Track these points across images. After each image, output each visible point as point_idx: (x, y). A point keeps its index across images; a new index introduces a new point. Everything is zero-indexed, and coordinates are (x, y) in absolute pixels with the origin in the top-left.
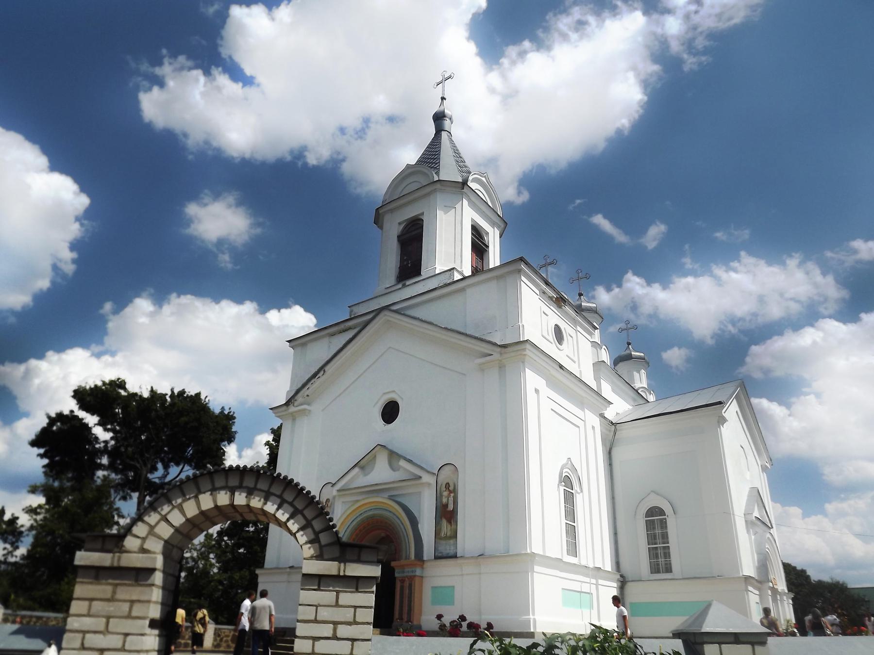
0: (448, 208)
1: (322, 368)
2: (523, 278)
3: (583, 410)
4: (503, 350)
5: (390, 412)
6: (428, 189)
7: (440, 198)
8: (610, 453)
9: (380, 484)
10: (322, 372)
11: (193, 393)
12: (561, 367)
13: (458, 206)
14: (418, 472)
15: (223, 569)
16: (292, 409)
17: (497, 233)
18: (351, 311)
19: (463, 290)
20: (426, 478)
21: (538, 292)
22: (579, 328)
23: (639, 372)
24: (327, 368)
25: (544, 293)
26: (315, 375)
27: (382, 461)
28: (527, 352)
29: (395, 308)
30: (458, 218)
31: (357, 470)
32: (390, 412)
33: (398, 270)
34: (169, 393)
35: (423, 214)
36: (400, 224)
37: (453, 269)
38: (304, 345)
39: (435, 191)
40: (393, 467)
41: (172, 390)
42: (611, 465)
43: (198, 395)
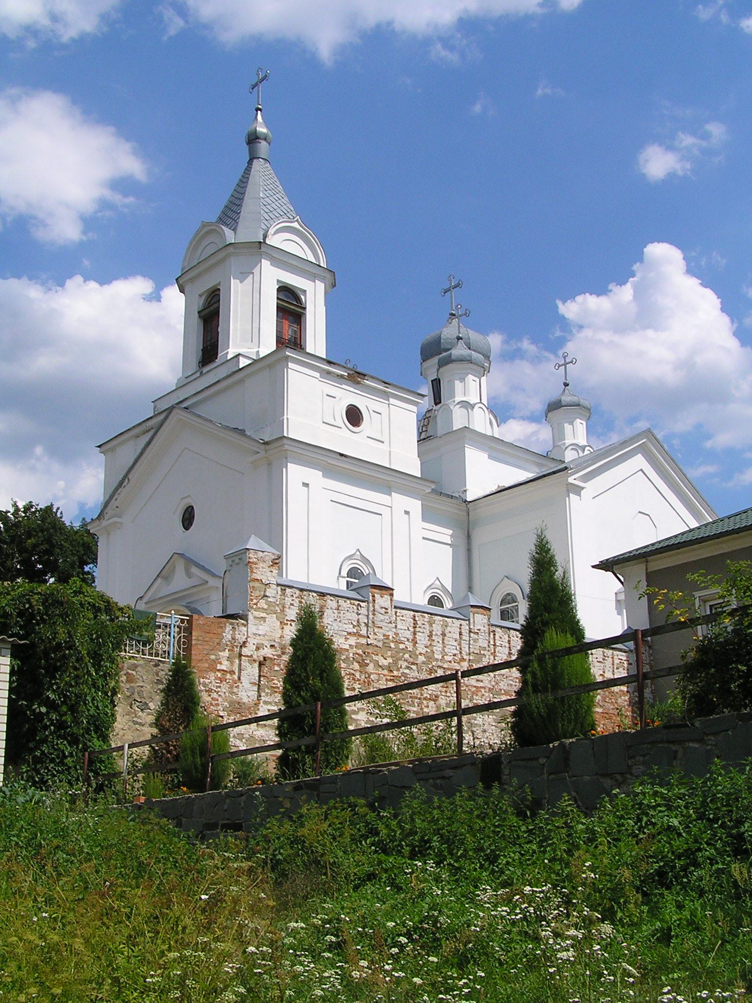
0: (243, 276)
1: (126, 476)
2: (291, 365)
3: (390, 495)
4: (267, 447)
5: (188, 518)
6: (221, 255)
7: (234, 263)
8: (469, 537)
9: (182, 591)
10: (127, 480)
11: (42, 506)
12: (342, 455)
13: (256, 271)
14: (206, 577)
15: (437, 956)
16: (104, 523)
17: (320, 286)
18: (155, 407)
19: (242, 381)
20: (213, 582)
21: (317, 375)
22: (392, 401)
23: (571, 423)
24: (130, 476)
25: (329, 373)
26: (121, 484)
27: (180, 566)
28: (286, 447)
29: (165, 414)
30: (257, 285)
31: (159, 580)
32: (188, 518)
33: (201, 353)
34: (12, 510)
35: (219, 284)
36: (200, 296)
37: (239, 354)
38: (113, 449)
39: (228, 256)
40: (189, 575)
41: (15, 505)
42: (469, 550)
43: (49, 509)
